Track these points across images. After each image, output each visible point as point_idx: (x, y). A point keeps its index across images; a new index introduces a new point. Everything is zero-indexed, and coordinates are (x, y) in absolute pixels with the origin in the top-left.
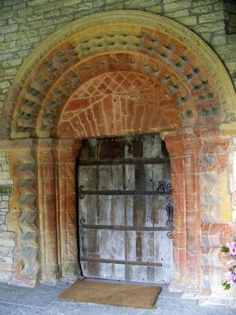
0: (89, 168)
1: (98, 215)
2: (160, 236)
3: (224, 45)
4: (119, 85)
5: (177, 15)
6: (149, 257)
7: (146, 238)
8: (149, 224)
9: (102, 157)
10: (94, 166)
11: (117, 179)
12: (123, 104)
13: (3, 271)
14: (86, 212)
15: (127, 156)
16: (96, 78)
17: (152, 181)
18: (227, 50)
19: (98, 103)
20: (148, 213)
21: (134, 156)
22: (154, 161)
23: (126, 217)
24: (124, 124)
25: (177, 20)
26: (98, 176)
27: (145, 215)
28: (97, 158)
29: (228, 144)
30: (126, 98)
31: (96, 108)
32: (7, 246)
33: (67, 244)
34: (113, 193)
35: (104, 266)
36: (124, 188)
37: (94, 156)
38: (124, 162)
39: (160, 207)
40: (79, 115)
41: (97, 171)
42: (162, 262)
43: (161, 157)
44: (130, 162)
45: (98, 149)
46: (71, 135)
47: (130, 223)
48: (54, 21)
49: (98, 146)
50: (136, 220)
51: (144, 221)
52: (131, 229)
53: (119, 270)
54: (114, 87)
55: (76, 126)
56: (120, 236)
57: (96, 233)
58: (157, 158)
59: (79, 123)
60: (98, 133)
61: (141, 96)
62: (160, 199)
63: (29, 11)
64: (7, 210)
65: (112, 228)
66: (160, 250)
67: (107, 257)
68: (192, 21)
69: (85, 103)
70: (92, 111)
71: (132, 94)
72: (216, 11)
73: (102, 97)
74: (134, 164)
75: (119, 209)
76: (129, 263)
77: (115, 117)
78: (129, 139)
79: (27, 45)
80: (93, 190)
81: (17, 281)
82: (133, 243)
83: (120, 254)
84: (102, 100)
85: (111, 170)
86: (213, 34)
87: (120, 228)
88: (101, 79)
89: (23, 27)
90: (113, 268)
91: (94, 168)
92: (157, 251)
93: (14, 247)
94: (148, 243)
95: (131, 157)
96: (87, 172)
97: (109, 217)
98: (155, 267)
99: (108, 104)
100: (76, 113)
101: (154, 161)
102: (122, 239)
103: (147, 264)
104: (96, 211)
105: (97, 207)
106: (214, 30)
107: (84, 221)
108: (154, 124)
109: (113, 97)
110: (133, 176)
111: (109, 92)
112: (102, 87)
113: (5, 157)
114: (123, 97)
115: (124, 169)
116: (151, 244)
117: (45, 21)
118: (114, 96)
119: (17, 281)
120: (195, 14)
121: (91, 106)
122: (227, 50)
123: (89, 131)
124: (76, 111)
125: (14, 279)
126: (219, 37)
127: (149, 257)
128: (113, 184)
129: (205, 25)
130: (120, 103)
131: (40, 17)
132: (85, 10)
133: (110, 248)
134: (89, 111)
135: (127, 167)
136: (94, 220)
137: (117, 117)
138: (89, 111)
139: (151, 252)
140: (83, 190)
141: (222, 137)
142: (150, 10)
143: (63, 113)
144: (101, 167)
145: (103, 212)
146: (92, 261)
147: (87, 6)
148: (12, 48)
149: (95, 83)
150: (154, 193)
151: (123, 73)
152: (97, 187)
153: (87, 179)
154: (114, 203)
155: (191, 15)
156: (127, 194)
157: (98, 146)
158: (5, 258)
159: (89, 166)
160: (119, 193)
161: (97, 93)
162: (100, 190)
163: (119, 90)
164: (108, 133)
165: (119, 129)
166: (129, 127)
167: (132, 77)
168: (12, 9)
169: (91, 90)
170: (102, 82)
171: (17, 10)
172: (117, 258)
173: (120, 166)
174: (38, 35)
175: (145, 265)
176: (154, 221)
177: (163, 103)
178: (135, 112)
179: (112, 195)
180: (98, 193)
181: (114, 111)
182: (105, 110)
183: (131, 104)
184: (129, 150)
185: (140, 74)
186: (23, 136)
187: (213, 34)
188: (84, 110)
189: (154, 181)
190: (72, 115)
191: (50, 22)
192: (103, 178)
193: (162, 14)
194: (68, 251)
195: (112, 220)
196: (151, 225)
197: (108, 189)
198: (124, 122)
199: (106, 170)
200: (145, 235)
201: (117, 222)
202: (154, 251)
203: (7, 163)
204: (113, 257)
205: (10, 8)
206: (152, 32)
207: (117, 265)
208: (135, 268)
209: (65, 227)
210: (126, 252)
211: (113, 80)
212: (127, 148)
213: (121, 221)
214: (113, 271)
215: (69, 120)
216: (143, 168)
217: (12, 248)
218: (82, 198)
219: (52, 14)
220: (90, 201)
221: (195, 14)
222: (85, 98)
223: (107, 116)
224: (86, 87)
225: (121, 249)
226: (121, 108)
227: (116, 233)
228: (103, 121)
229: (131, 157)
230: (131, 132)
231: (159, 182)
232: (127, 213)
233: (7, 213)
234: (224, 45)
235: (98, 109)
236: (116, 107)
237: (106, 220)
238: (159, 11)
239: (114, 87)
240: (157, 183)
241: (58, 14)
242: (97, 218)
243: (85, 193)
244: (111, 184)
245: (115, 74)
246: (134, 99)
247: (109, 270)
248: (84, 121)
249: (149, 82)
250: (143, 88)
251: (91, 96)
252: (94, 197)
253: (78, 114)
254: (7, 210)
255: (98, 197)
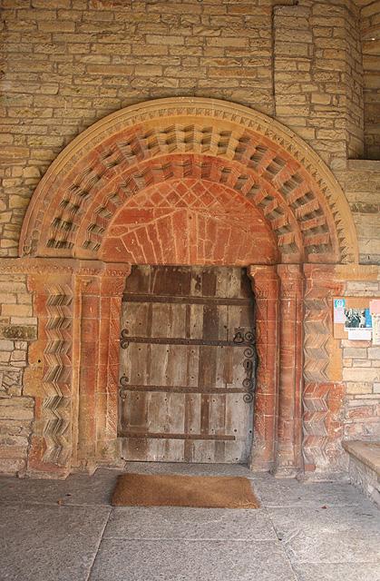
0: (138, 306)
1: (148, 372)
2: (234, 400)
3: (344, 170)
4: (198, 198)
5: (292, 122)
6: (219, 428)
7: (215, 404)
8: (220, 384)
9: (158, 291)
10: (146, 304)
11: (178, 322)
12: (202, 224)
13: (10, 457)
14: (130, 368)
15: (194, 293)
16: (165, 182)
17: (225, 327)
18: (347, 177)
19: (166, 218)
20: (220, 370)
21: (203, 293)
22: (229, 302)
23: (188, 375)
24: (201, 250)
25: (293, 128)
26: (150, 317)
27: (215, 373)
28: (150, 292)
29: (341, 289)
30: (206, 216)
31: (162, 224)
32: (20, 419)
33: (106, 412)
34: (171, 341)
35: (154, 443)
36: (188, 335)
37: (146, 290)
38: (190, 301)
39: (236, 363)
40: (137, 232)
41: (150, 309)
42: (235, 434)
43: (240, 297)
44: (198, 301)
45: (152, 280)
46: (122, 258)
47: (194, 383)
48: (118, 92)
49: (153, 275)
50: (203, 378)
51: (213, 381)
52: (195, 390)
53: (176, 448)
54: (191, 199)
55: (131, 247)
56: (178, 401)
57: (143, 397)
58: (235, 298)
59: (135, 242)
60: (163, 259)
61: (227, 217)
62: (235, 351)
63: (80, 69)
64: (24, 364)
65: (168, 389)
66: (233, 419)
67: (159, 430)
68: (309, 134)
69: (147, 216)
70: (156, 228)
71: (215, 211)
72: (337, 129)
73: (172, 210)
74: (203, 303)
75: (179, 364)
76: (190, 438)
77: (189, 239)
78: (197, 270)
79: (73, 119)
80: (142, 336)
81: (35, 471)
82: (197, 410)
83: (178, 424)
84: (171, 214)
85: (171, 310)
86: (333, 156)
87: (180, 390)
88: (172, 185)
89: (66, 92)
90: (167, 446)
91: (145, 307)
92: (229, 420)
93: (34, 420)
94: (218, 410)
95: (200, 294)
96: (134, 312)
97: (164, 374)
98: (226, 442)
99: (180, 221)
100: (132, 228)
101: (229, 302)
102: (181, 405)
103: (216, 437)
104: (146, 366)
105: (147, 361)
106: (334, 150)
107: (127, 380)
108: (242, 256)
109: (188, 213)
110: (202, 321)
111: (182, 205)
112: (173, 197)
113: (26, 283)
114: (203, 214)
115: (189, 310)
116: (222, 410)
117: (103, 90)
118: (189, 212)
119: (35, 471)
120: (312, 126)
121: (155, 221)
122: (347, 177)
123: (149, 254)
124: (132, 225)
125: (29, 469)
126: (339, 160)
127: (219, 428)
128: (173, 330)
129: (326, 142)
130: (197, 223)
131: (96, 82)
132: (167, 88)
133: (164, 418)
134: (151, 227)
135: (193, 307)
136: (142, 379)
137: (192, 240)
138: (151, 227)
139: (222, 421)
140: (127, 335)
141: (336, 280)
142: (257, 107)
143: (110, 225)
144: (155, 305)
145: (155, 368)
146: (135, 436)
147: (170, 83)
148: (46, 119)
149: (163, 190)
150: (228, 343)
151: (203, 182)
152: (149, 333)
153: (134, 322)
154: (172, 356)
155: (309, 126)
156: (139, 342)
157: (153, 276)
158: (14, 438)
159: (139, 303)
160: (181, 341)
161: (165, 204)
162: (152, 336)
163: (196, 205)
164: (177, 262)
165: (194, 257)
166: (208, 255)
167: (215, 189)
168: (48, 60)
169: (156, 198)
170: (173, 190)
171: (58, 64)
172: (173, 431)
173: (183, 306)
174: (92, 108)
175: (212, 439)
176: (228, 380)
177: (253, 229)
178: (217, 236)
179: (197, 303)
180: (149, 341)
181: (188, 232)
182: (176, 228)
183: (212, 225)
184: (197, 286)
185: (227, 187)
186: (60, 254)
187: (333, 156)
188: (145, 225)
189: (229, 328)
190: (126, 230)
191: (112, 93)
192: (158, 321)
193: (273, 117)
194: (107, 424)
195: (169, 379)
196: (223, 386)
197: (164, 336)
198: (202, 248)
199: (163, 309)
200: (213, 399)
201: (175, 381)
202: (225, 419)
203: (28, 292)
204: (168, 430)
205: (108, 59)
206: (259, 138)
207: (172, 441)
208: (198, 444)
209: (105, 388)
210: (186, 422)
211: (190, 190)
212: (194, 282)
213: (181, 380)
214: (167, 449)
215: (120, 237)
216: (215, 310)
217: (29, 422)
218: (125, 347)
219: (114, 82)
220: (137, 353)
221: (312, 126)
222: (146, 209)
223: (178, 238)
224: (149, 192)
225: (180, 418)
226: (198, 229)
227: (173, 396)
228: (172, 244)
229: (200, 294)
230: (209, 262)
231: (236, 329)
232: (191, 369)
233: (24, 368)
234: (344, 170)
235: (166, 226)
236: (191, 227)
237: (160, 379)
238: (270, 112)
239: (191, 199)
240: (233, 332)
241: (125, 84)
242: (146, 375)
243: (131, 340)
244: (169, 329)
245: (193, 182)
246: (216, 218)
247: (160, 449)
248: (143, 240)
249: (238, 199)
250: (229, 206)
251: (156, 206)
252: (142, 346)
253: (134, 230)
254: (24, 364)
255: (149, 346)
